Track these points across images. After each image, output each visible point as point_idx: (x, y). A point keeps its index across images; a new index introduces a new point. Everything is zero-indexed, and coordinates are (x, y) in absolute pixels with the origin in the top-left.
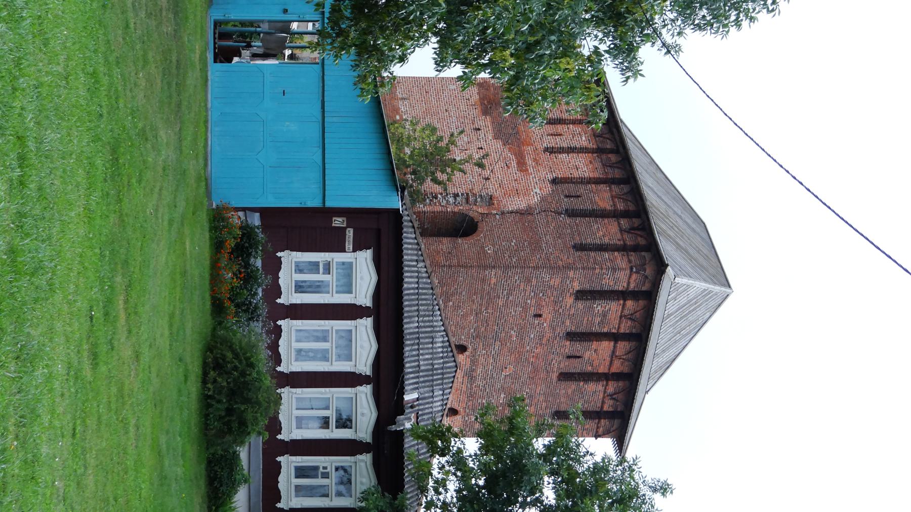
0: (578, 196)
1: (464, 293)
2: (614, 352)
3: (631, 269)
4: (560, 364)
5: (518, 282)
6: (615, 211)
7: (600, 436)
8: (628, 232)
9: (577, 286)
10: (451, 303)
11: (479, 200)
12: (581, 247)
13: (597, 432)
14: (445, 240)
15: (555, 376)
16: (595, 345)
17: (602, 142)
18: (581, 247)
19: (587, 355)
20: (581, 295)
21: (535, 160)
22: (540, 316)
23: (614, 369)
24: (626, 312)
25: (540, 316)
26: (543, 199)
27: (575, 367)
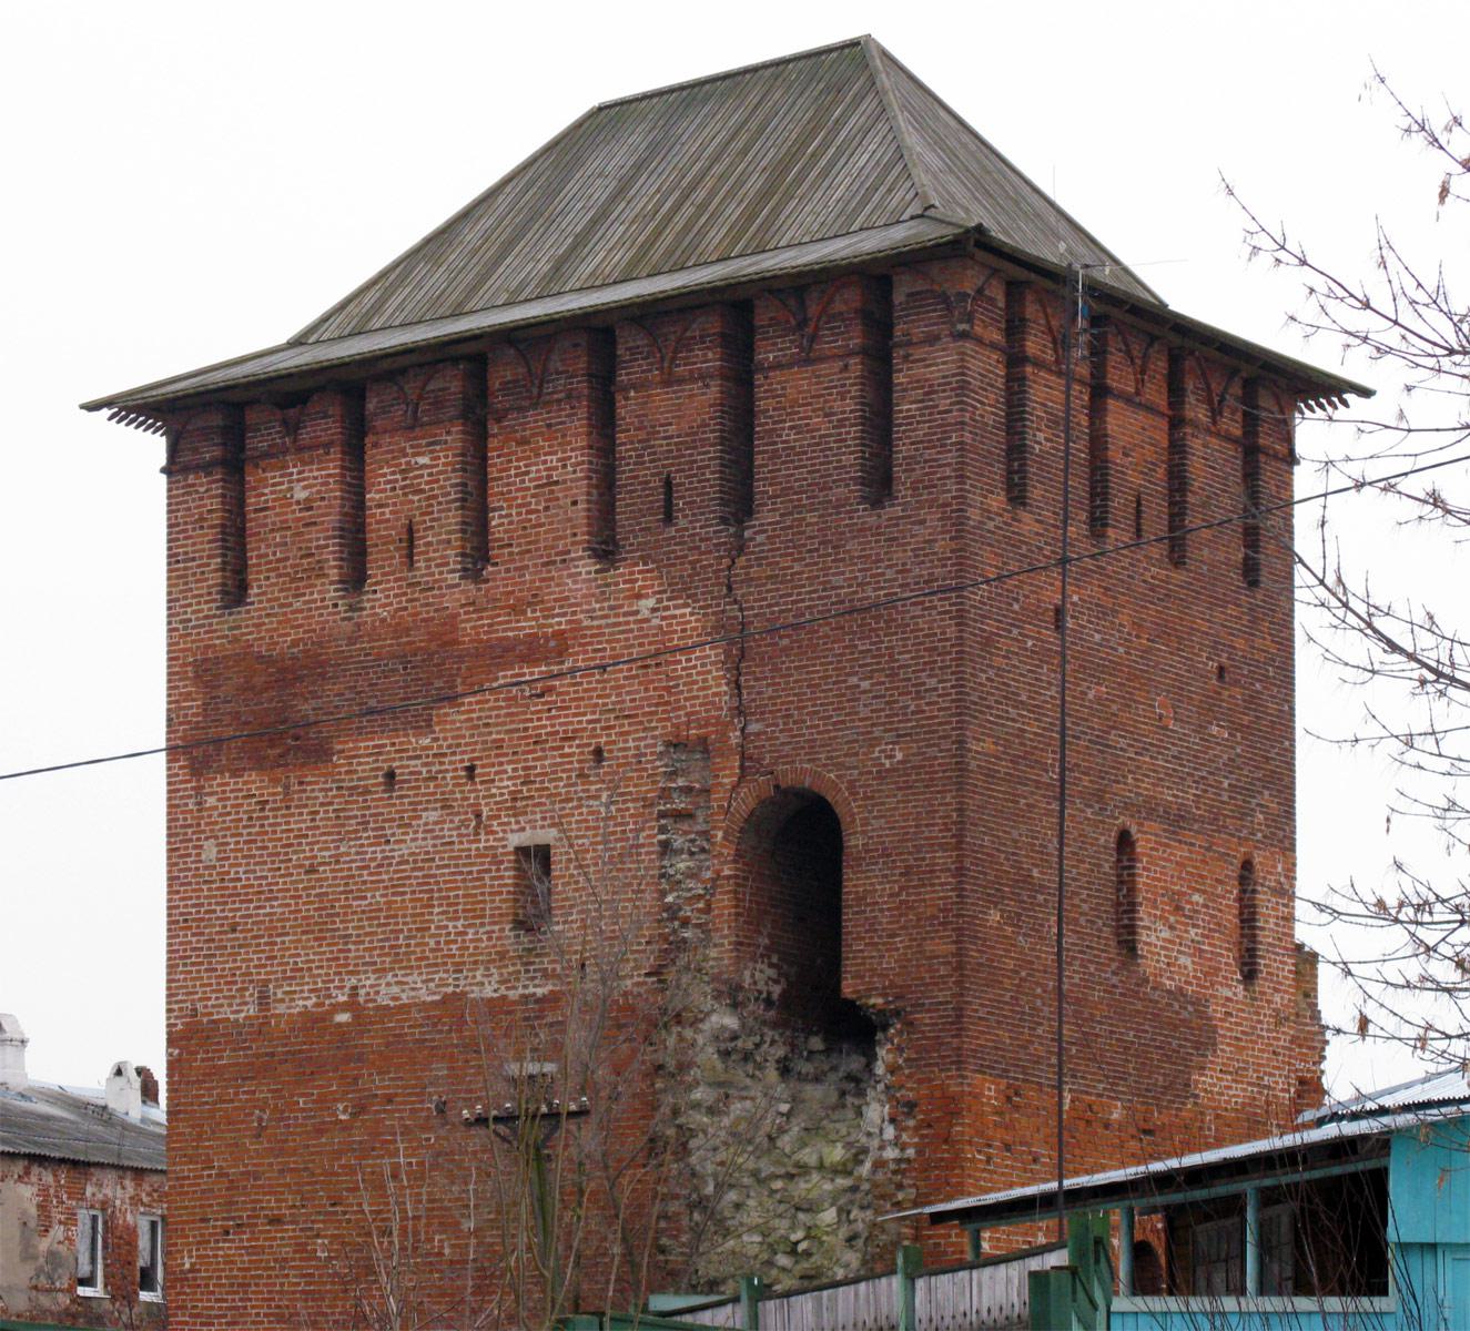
0: (668, 484)
1: (1015, 834)
2: (1129, 400)
3: (964, 335)
4: (1151, 565)
5: (991, 673)
6: (723, 377)
7: (1292, 451)
8: (813, 338)
9: (997, 501)
10: (1035, 873)
11: (681, 782)
12: (879, 483)
13: (1283, 460)
14: (853, 883)
15: (1179, 576)
16: (1114, 454)
17: (438, 404)
18: (879, 483)
19: (1135, 479)
20: (1017, 496)
21: (517, 610)
23: (1161, 401)
24: (1050, 356)
26: (682, 590)
27: (1156, 519)
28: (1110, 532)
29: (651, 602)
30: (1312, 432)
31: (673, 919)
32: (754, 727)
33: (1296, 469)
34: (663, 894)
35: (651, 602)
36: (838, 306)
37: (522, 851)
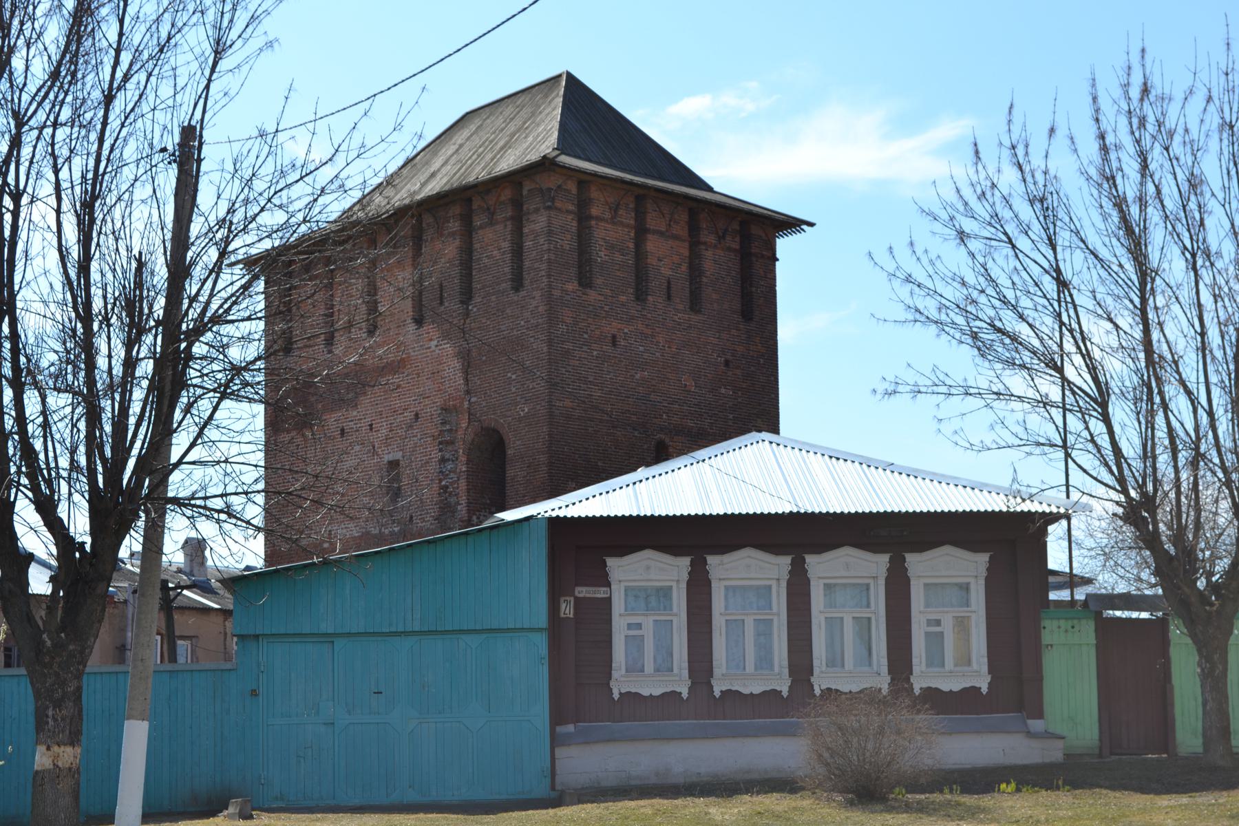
2: (661, 234)
8: (493, 214)
11: (448, 427)
14: (510, 473)
18: (518, 282)
19: (667, 272)
22: (614, 337)
24: (608, 215)
25: (614, 337)
26: (446, 336)
28: (650, 298)
29: (435, 343)
30: (785, 246)
31: (445, 492)
32: (473, 400)
33: (777, 263)
34: (440, 480)
35: (435, 343)
36: (503, 198)
37: (390, 463)
